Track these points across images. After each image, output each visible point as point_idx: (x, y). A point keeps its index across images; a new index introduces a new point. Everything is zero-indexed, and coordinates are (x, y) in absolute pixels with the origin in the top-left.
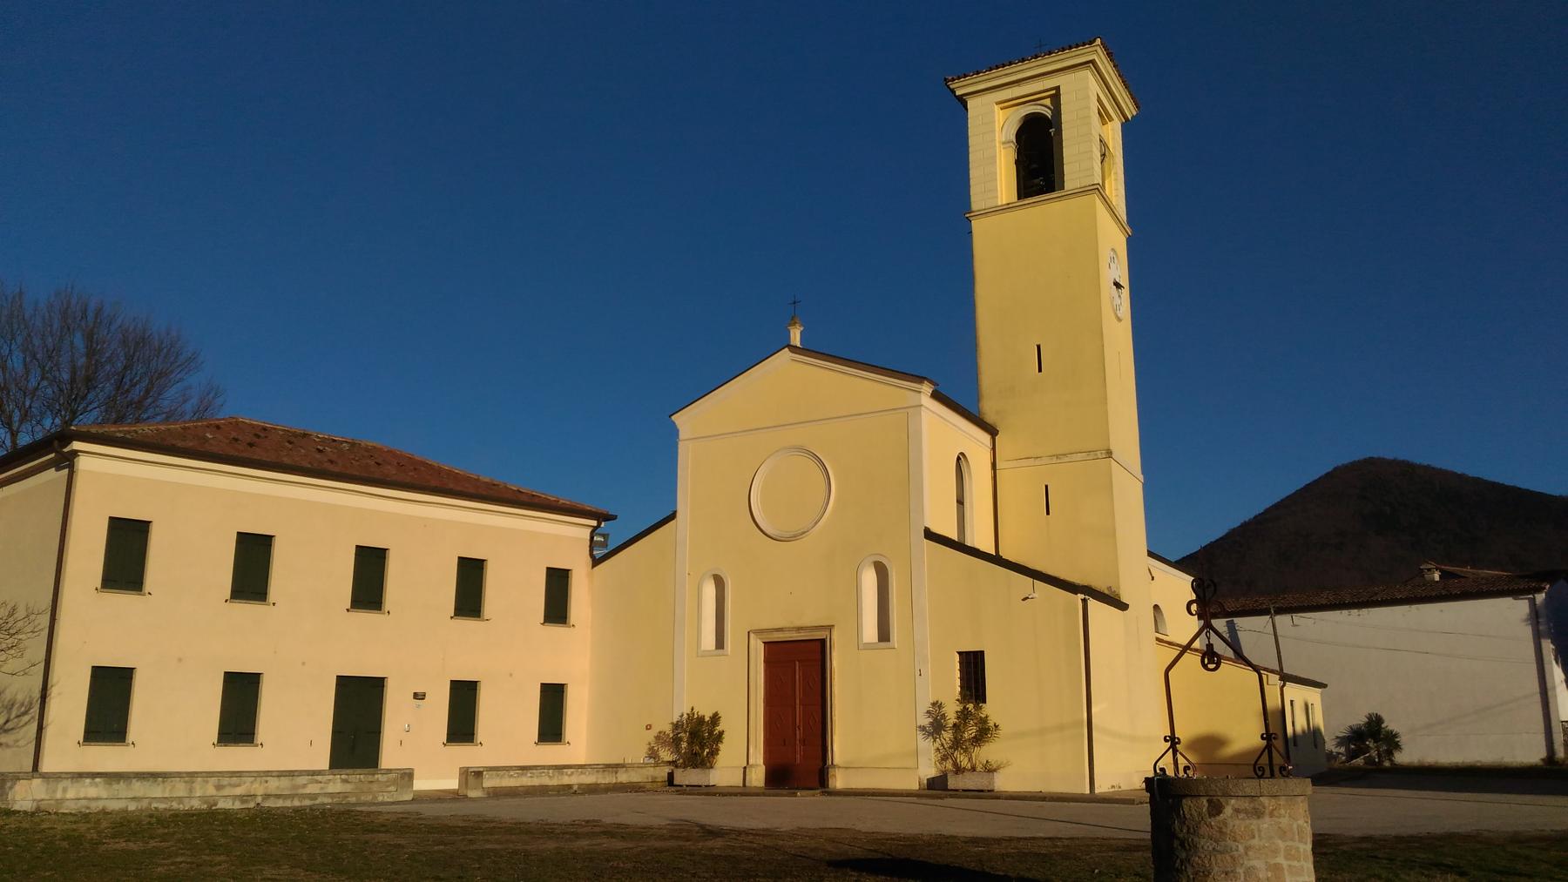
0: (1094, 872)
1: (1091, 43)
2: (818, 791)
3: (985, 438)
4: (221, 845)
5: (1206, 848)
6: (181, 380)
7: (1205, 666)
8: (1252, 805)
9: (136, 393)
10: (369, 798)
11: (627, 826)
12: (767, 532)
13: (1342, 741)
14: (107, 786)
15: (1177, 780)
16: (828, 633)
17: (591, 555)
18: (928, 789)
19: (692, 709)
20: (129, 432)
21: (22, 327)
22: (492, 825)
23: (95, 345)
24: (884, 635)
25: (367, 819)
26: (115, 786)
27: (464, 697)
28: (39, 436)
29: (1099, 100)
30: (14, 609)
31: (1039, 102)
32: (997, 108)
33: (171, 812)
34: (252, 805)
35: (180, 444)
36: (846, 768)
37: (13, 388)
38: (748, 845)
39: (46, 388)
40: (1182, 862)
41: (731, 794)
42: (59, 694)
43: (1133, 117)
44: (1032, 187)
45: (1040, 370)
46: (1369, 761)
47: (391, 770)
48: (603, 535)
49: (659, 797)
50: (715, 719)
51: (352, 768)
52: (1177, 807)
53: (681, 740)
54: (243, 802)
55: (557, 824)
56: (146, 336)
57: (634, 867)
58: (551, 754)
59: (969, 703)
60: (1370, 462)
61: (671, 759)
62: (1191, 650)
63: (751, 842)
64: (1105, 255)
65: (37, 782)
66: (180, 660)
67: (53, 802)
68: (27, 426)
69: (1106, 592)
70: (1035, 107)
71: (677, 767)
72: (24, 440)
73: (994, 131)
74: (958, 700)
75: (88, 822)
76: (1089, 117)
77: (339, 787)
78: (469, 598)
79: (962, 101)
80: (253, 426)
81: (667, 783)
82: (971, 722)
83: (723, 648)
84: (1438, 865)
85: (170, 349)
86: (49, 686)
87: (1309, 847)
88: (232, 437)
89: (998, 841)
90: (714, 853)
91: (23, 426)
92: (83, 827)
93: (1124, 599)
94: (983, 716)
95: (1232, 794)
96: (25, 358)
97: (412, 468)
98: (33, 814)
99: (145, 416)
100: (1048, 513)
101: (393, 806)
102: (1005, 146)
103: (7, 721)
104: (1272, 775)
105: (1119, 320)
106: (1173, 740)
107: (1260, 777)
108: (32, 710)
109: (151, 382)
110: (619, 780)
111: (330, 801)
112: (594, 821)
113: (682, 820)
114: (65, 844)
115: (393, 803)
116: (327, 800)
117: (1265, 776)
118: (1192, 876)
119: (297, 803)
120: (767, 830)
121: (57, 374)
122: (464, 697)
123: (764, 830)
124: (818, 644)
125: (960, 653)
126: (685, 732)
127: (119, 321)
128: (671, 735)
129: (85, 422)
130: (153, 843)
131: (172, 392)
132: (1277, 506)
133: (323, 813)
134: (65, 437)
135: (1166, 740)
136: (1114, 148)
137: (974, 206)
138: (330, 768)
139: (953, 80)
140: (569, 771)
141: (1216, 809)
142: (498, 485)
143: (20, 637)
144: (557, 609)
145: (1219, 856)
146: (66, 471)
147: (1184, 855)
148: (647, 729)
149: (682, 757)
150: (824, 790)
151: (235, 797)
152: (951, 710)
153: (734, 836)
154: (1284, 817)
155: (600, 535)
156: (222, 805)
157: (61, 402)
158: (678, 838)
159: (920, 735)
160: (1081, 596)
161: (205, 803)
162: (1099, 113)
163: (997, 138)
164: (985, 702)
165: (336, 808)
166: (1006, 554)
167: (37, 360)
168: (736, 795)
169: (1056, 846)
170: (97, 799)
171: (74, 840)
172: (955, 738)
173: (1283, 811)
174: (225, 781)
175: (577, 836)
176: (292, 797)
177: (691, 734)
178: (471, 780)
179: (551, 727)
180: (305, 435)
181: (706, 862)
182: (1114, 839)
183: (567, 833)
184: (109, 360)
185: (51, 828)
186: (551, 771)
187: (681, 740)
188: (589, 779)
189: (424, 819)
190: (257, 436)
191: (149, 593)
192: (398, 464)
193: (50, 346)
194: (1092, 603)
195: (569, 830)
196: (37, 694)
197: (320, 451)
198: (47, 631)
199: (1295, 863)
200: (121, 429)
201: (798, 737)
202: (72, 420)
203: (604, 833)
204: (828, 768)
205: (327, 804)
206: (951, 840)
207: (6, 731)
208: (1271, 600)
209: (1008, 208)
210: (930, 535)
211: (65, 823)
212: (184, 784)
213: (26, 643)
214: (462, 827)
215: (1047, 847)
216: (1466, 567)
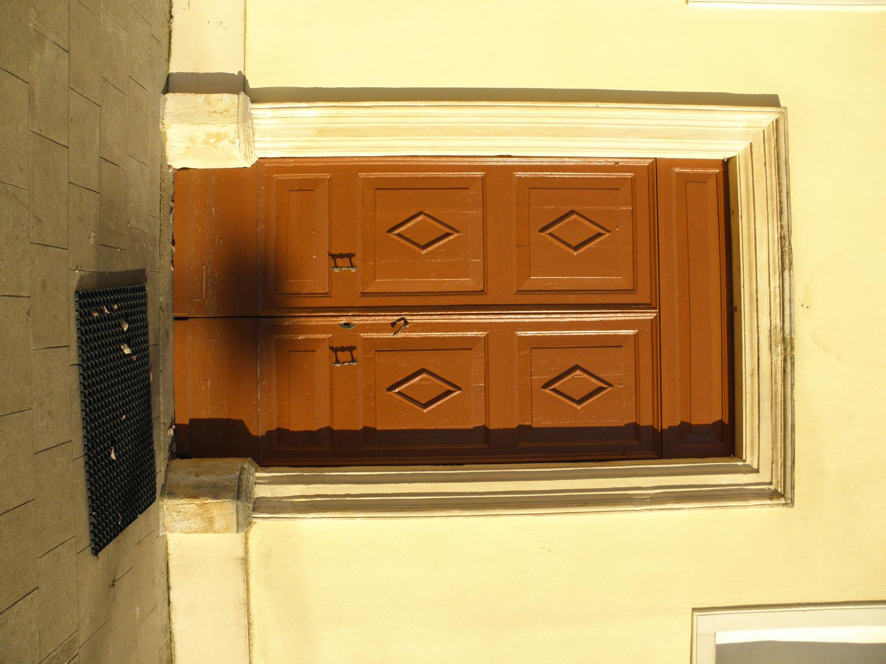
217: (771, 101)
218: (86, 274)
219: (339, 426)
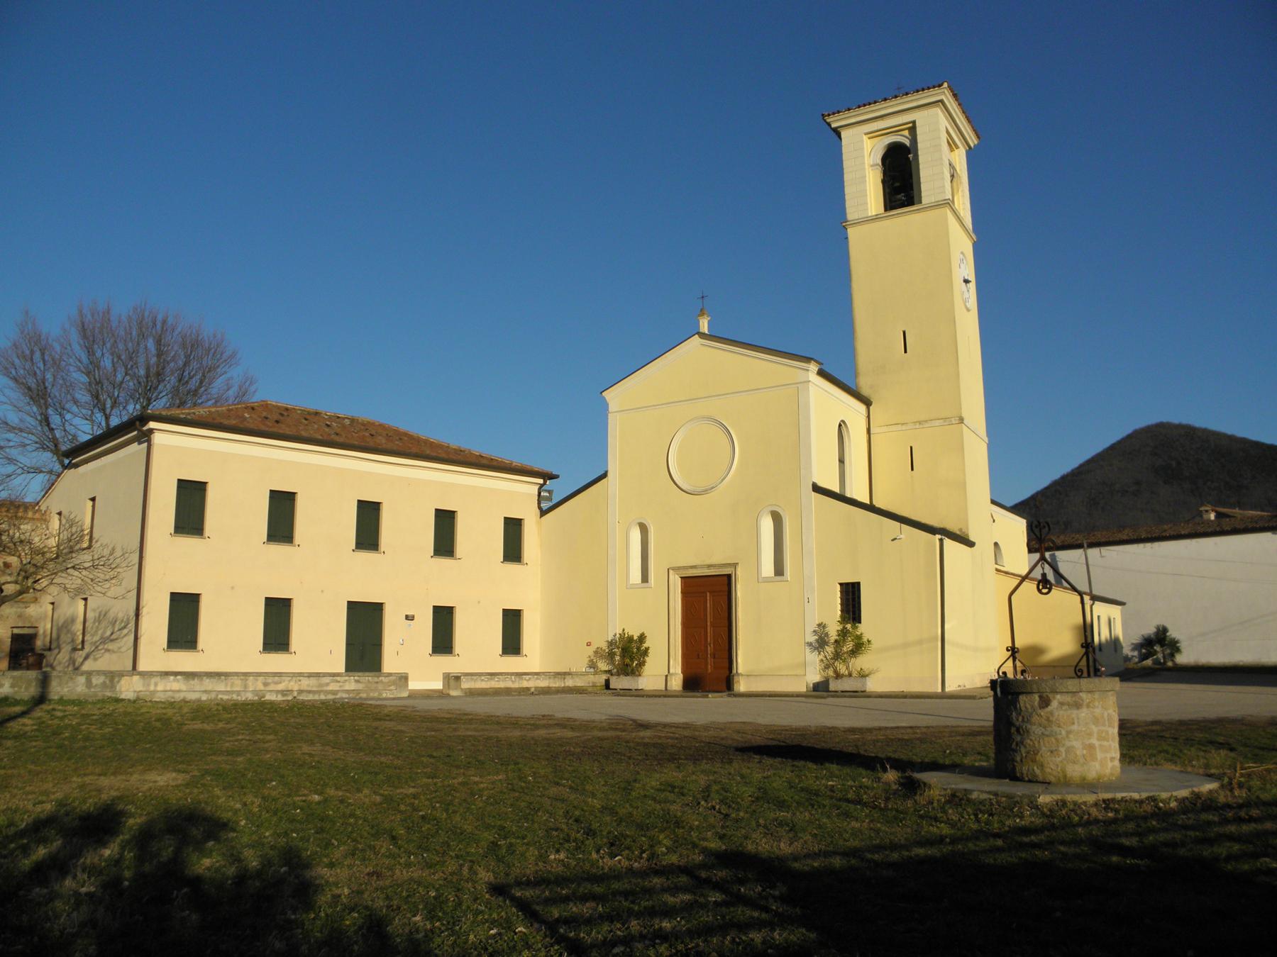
0: (945, 752)
1: (940, 86)
2: (724, 694)
3: (862, 408)
4: (269, 728)
5: (1036, 732)
6: (225, 372)
7: (1040, 591)
8: (1074, 699)
9: (193, 384)
10: (376, 695)
11: (575, 720)
12: (682, 487)
13: (1137, 647)
14: (185, 682)
15: (1016, 681)
17: (540, 508)
18: (814, 691)
19: (624, 630)
20: (189, 414)
21: (110, 335)
22: (470, 717)
23: (162, 348)
24: (779, 571)
25: (377, 710)
26: (192, 682)
27: (443, 619)
28: (125, 418)
29: (948, 132)
30: (113, 549)
31: (900, 133)
32: (865, 137)
33: (232, 702)
34: (290, 698)
35: (226, 422)
36: (748, 675)
37: (106, 383)
38: (672, 735)
39: (129, 381)
40: (1017, 744)
41: (656, 696)
42: (148, 613)
43: (974, 146)
44: (896, 201)
45: (906, 352)
46: (1156, 662)
47: (391, 673)
48: (550, 492)
49: (598, 698)
50: (642, 638)
51: (362, 671)
52: (1014, 702)
53: (614, 654)
54: (284, 695)
55: (520, 717)
56: (200, 339)
57: (582, 751)
58: (512, 664)
59: (847, 623)
60: (1161, 426)
61: (607, 669)
62: (1019, 576)
63: (673, 733)
64: (956, 257)
65: (136, 678)
66: (233, 588)
67: (148, 693)
68: (116, 411)
69: (958, 533)
70: (896, 137)
71: (612, 675)
72: (115, 422)
73: (863, 156)
74: (839, 621)
75: (174, 708)
76: (940, 145)
77: (352, 686)
78: (445, 543)
79: (837, 132)
80: (278, 407)
82: (849, 638)
83: (648, 582)
84: (1212, 743)
85: (216, 350)
86: (141, 607)
87: (1116, 730)
88: (263, 415)
89: (870, 730)
90: (645, 741)
91: (113, 411)
92: (170, 712)
93: (972, 538)
94: (859, 633)
95: (1058, 690)
96: (113, 359)
97: (397, 438)
98: (134, 702)
99: (200, 401)
100: (912, 469)
101: (395, 701)
102: (873, 168)
103: (112, 634)
104: (1089, 676)
105: (968, 310)
106: (1013, 651)
107: (1079, 677)
108: (130, 625)
109: (204, 376)
110: (567, 684)
111: (347, 696)
112: (548, 715)
113: (617, 716)
114: (158, 724)
115: (394, 699)
116: (345, 695)
117: (1083, 676)
118: (1024, 755)
119: (323, 697)
120: (686, 724)
121: (137, 371)
122: (443, 619)
123: (683, 724)
124: (726, 578)
125: (841, 584)
126: (618, 648)
127: (179, 329)
128: (607, 650)
129: (158, 406)
130: (221, 725)
131: (219, 384)
132: (1089, 462)
133: (343, 705)
134: (143, 419)
135: (1008, 650)
136: (961, 170)
137: (850, 217)
138: (346, 671)
139: (829, 115)
140: (527, 677)
141: (1045, 702)
142: (464, 451)
143: (119, 570)
144: (513, 552)
145: (1046, 739)
146: (145, 444)
147: (1019, 738)
148: (587, 645)
149: (616, 667)
150: (730, 693)
151: (278, 692)
152: (833, 629)
153: (660, 728)
154: (1098, 707)
155: (546, 491)
156: (269, 697)
157: (140, 392)
158: (616, 729)
159: (808, 650)
160: (938, 536)
161: (257, 695)
162: (948, 142)
163: (866, 162)
164: (860, 622)
165: (352, 701)
166: (878, 503)
167: (122, 360)
168: (660, 696)
169: (917, 733)
170: (179, 691)
171: (165, 721)
172: (836, 651)
173: (1097, 704)
174: (270, 680)
175: (536, 727)
176: (319, 692)
177: (623, 649)
178: (452, 682)
179: (512, 644)
180: (317, 414)
181: (638, 748)
182: (961, 727)
183: (528, 724)
184: (173, 359)
185: (148, 712)
186: (513, 677)
187: (614, 654)
188: (543, 683)
189: (418, 711)
190: (282, 415)
191: (209, 537)
192: (387, 435)
193: (131, 350)
194: (947, 542)
195: (529, 722)
196: (132, 613)
197: (328, 425)
198: (137, 566)
199: (1105, 743)
200: (183, 411)
201: (709, 652)
202: (148, 405)
203: (557, 725)
204: (733, 676)
205: (346, 698)
206: (833, 730)
207: (112, 641)
208: (1084, 537)
209: (876, 218)
210: (817, 489)
211: (157, 708)
212: (240, 681)
213: (124, 574)
214: (447, 718)
215: (908, 734)
216: (1235, 509)
217: (668, 569)
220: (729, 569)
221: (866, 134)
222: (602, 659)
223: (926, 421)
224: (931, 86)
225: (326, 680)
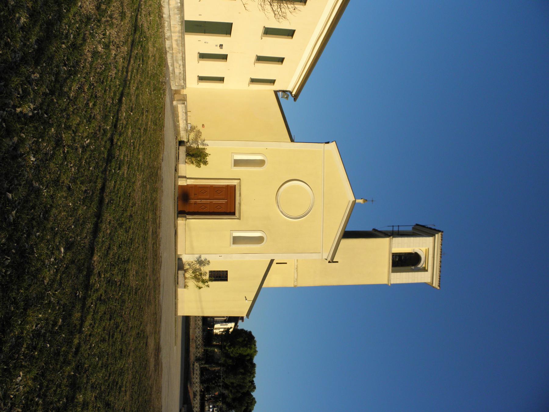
16: (237, 217)
18: (178, 258)
31: (424, 264)
61: (190, 139)
81: (180, 140)
124: (233, 211)
138: (186, 21)
139: (442, 235)
159: (197, 256)
170: (169, 4)
217: (240, 179)
218: (229, 329)
219: (195, 211)
220: (238, 215)
221: (428, 249)
222: (195, 136)
223: (297, 271)
224: (442, 255)
225: (181, 62)
